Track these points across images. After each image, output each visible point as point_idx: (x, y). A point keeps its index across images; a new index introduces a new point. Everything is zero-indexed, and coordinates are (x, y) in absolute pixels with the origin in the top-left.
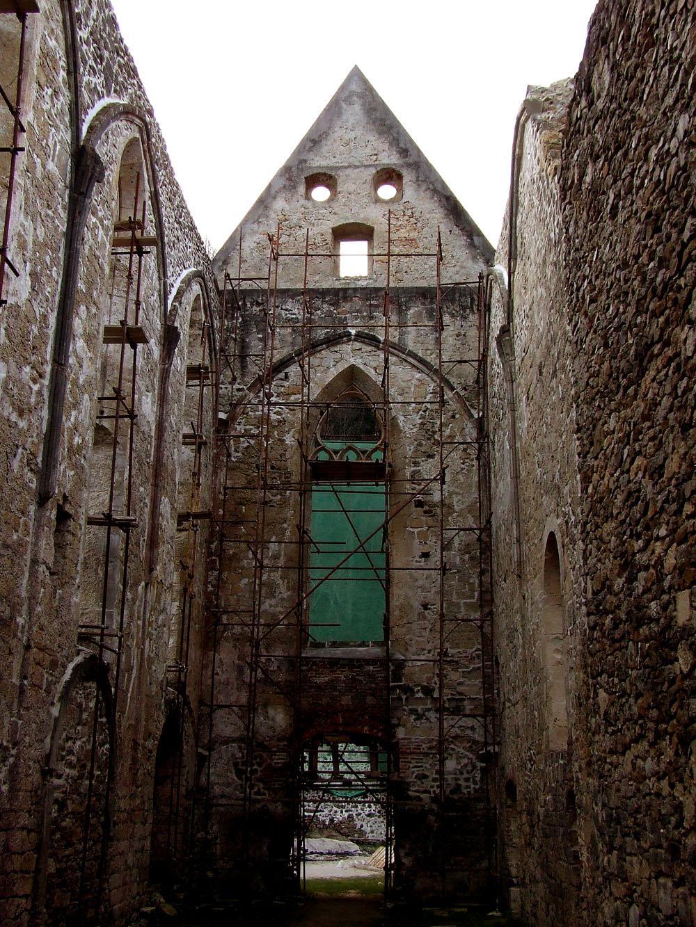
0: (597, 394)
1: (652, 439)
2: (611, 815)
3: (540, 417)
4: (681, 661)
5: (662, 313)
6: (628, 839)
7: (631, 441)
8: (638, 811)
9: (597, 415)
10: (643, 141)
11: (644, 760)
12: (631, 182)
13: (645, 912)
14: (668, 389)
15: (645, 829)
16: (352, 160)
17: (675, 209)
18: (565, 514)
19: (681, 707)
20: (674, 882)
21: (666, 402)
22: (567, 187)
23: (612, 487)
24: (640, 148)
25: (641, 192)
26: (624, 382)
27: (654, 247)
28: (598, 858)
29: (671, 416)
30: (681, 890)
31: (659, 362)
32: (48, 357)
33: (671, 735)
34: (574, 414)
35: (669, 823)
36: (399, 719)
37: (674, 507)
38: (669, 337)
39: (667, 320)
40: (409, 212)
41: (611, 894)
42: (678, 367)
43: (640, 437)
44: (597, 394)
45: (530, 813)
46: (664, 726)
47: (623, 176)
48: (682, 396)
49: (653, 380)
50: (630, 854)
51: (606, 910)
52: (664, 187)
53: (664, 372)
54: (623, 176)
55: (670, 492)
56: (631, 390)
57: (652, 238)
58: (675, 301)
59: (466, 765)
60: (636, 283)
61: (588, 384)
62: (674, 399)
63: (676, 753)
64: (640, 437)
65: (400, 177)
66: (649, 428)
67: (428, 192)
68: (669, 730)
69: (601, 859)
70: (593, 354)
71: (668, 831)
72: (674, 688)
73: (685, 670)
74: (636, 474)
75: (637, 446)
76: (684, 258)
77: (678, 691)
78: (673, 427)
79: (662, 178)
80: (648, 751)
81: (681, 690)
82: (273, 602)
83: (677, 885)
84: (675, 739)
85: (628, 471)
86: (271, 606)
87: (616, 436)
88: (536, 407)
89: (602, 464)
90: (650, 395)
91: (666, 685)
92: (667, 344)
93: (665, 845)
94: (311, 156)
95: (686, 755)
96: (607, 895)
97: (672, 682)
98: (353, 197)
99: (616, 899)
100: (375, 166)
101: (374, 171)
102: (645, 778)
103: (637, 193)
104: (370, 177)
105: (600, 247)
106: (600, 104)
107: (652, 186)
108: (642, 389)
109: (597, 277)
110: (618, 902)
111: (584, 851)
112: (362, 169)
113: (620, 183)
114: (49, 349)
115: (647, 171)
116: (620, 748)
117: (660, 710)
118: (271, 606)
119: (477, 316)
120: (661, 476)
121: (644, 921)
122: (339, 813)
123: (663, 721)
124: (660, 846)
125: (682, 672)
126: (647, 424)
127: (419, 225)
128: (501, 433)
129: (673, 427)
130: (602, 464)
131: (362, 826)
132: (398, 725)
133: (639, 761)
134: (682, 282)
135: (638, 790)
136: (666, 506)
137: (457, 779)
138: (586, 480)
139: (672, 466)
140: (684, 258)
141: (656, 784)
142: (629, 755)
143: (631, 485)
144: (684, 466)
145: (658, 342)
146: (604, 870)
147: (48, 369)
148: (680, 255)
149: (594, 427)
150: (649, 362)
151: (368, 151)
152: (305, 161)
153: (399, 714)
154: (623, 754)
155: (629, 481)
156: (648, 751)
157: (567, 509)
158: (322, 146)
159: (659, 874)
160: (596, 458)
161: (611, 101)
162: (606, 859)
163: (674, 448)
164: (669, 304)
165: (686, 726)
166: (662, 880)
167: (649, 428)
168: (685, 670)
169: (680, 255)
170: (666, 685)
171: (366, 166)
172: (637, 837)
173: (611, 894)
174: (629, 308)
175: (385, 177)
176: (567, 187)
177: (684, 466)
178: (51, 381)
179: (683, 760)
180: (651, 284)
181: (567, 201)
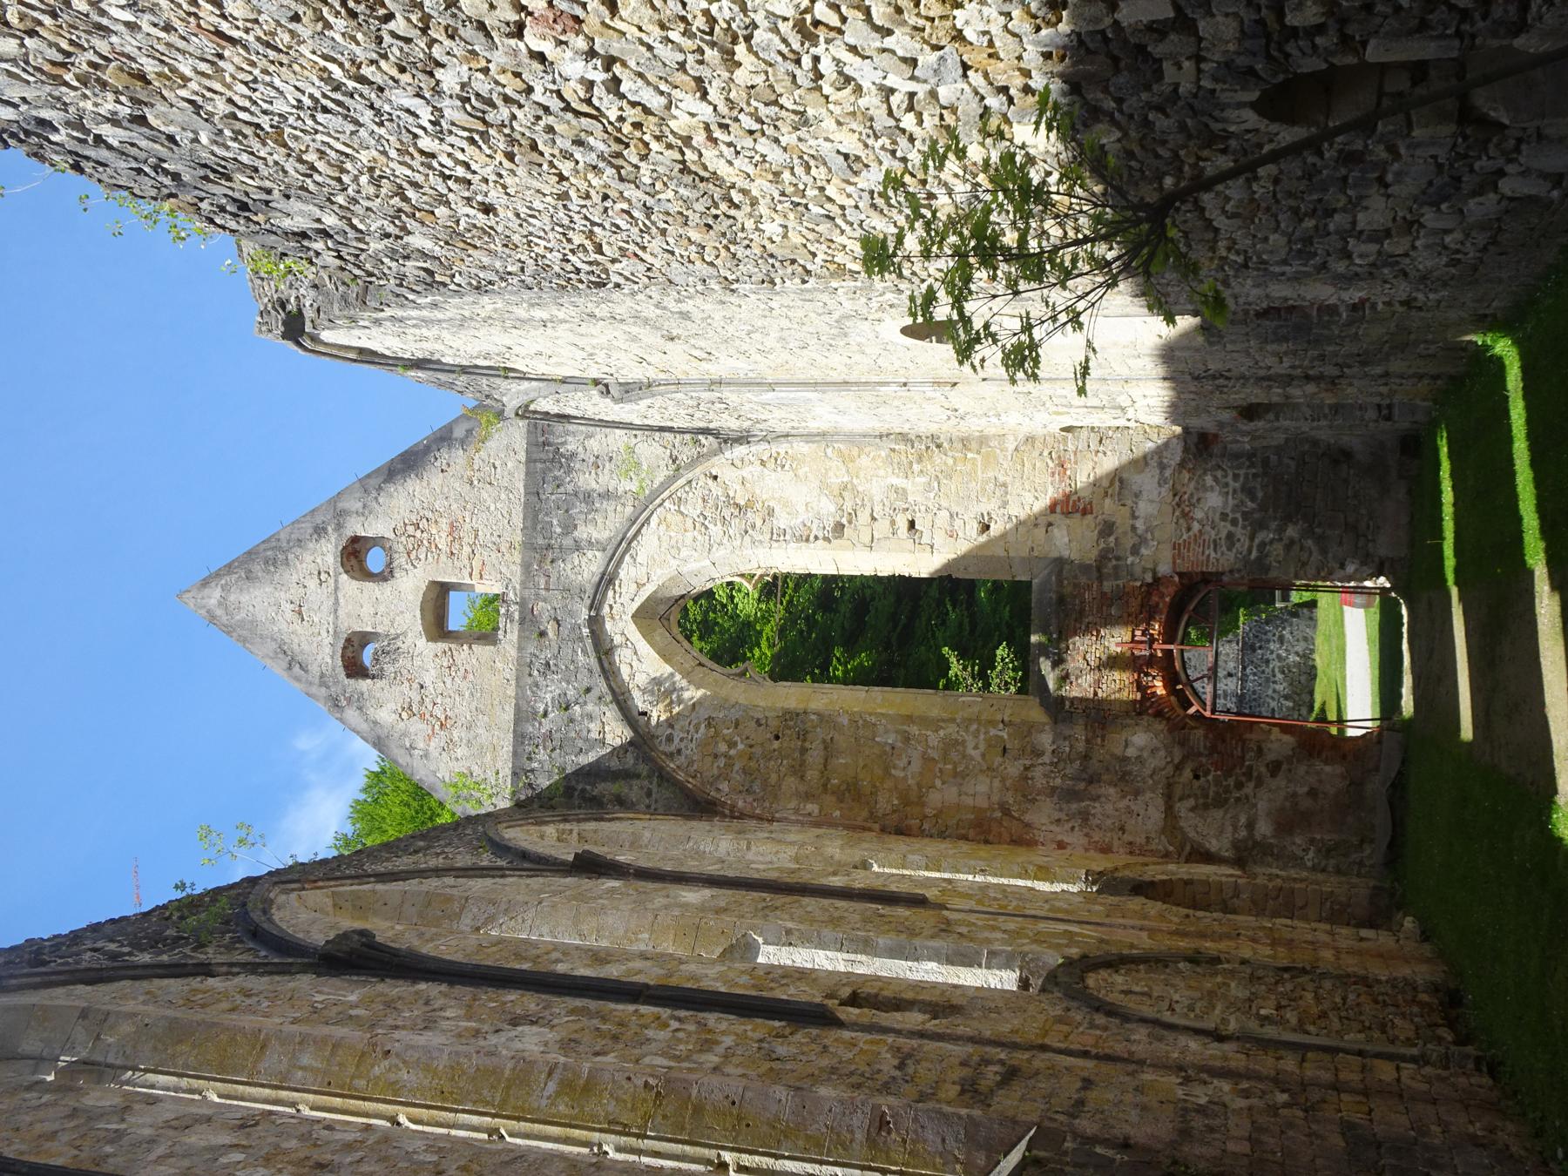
0: (728, 249)
1: (808, 168)
2: (1299, 251)
3: (738, 342)
4: (1104, 141)
5: (647, 145)
6: (1332, 227)
7: (804, 201)
8: (1295, 211)
9: (757, 251)
10: (407, 159)
11: (1228, 199)
12: (458, 180)
13: (1431, 204)
14: (748, 142)
15: (1320, 200)
16: (325, 608)
17: (514, 117)
18: (881, 308)
19: (1164, 143)
20: (1394, 160)
21: (764, 146)
22: (429, 280)
23: (858, 233)
24: (413, 163)
25: (474, 166)
26: (724, 206)
27: (556, 152)
28: (1357, 274)
29: (784, 141)
30: (1403, 151)
31: (709, 154)
32: (631, 1008)
33: (1199, 158)
34: (747, 286)
35: (1314, 165)
36: (1145, 570)
37: (903, 142)
38: (681, 138)
39: (658, 138)
40: (411, 529)
41: (1406, 255)
42: (724, 127)
43: (801, 187)
44: (728, 249)
45: (1288, 380)
46: (1186, 168)
47: (445, 191)
48: (763, 123)
49: (730, 163)
50: (1354, 223)
51: (1429, 264)
52: (477, 132)
53: (723, 148)
54: (445, 191)
55: (883, 148)
56: (736, 196)
57: (542, 154)
58: (637, 126)
59: (1216, 479)
60: (595, 182)
61: (711, 264)
62: (763, 134)
63: (1224, 151)
64: (801, 187)
65: (356, 539)
66: (793, 174)
67: (381, 500)
68: (1192, 160)
69: (1358, 269)
70: (672, 253)
71: (1326, 167)
72: (1137, 150)
73: (1118, 134)
74: (849, 196)
75: (811, 193)
76: (585, 108)
77: (1143, 147)
78: (800, 139)
79: (466, 134)
80: (1218, 194)
81: (1141, 142)
82: (970, 744)
83: (1397, 156)
84: (1205, 153)
85: (843, 208)
86: (976, 748)
87: (790, 225)
88: (723, 347)
89: (824, 247)
90: (750, 169)
91: (1133, 163)
92: (687, 140)
93: (1343, 171)
94: (314, 669)
95: (1227, 138)
96: (1407, 261)
97: (1130, 154)
98: (382, 609)
99: (1414, 248)
100: (337, 575)
101: (345, 576)
102: (1252, 200)
103: (474, 172)
104: (354, 582)
105: (531, 234)
106: (330, 220)
107: (470, 150)
108: (741, 183)
109: (569, 241)
110: (1418, 243)
111: (1345, 296)
112: (340, 595)
113: (451, 196)
114: (620, 1007)
115: (449, 155)
116: (1210, 236)
117: (1165, 174)
118: (976, 748)
119: (570, 439)
120: (858, 158)
121: (1444, 207)
122: (1277, 687)
123: (1181, 170)
124: (1345, 179)
125: (1119, 140)
126: (786, 175)
127: (430, 515)
128: (747, 407)
129: (800, 139)
130: (824, 247)
131: (1297, 654)
132: (1154, 572)
133: (1228, 208)
134: (613, 115)
135: (1268, 209)
136: (899, 154)
137: (1235, 491)
138: (841, 271)
139: (851, 145)
140: (585, 108)
141: (1262, 183)
142: (1220, 222)
143: (861, 205)
144: (854, 126)
145: (683, 154)
146: (1373, 265)
147: (645, 1009)
148: (577, 114)
149: (772, 256)
150: (705, 168)
151: (312, 584)
152: (322, 676)
153: (1138, 570)
154: (1217, 230)
155: (857, 207)
156: (1218, 194)
157: (874, 304)
158: (302, 652)
159: (1382, 182)
160: (814, 255)
161: (333, 203)
162: (1358, 261)
163: (827, 139)
164: (638, 134)
165: (1190, 137)
166: (1389, 178)
167: (793, 174)
168: (1118, 134)
169: (577, 114)
170: (1133, 163)
171: (336, 589)
172: (1330, 213)
173: (1406, 255)
174: (626, 194)
175: (353, 561)
176: (429, 280)
177: (854, 126)
178: (664, 1006)
179: (1233, 143)
180: (604, 159)
181: (448, 280)
